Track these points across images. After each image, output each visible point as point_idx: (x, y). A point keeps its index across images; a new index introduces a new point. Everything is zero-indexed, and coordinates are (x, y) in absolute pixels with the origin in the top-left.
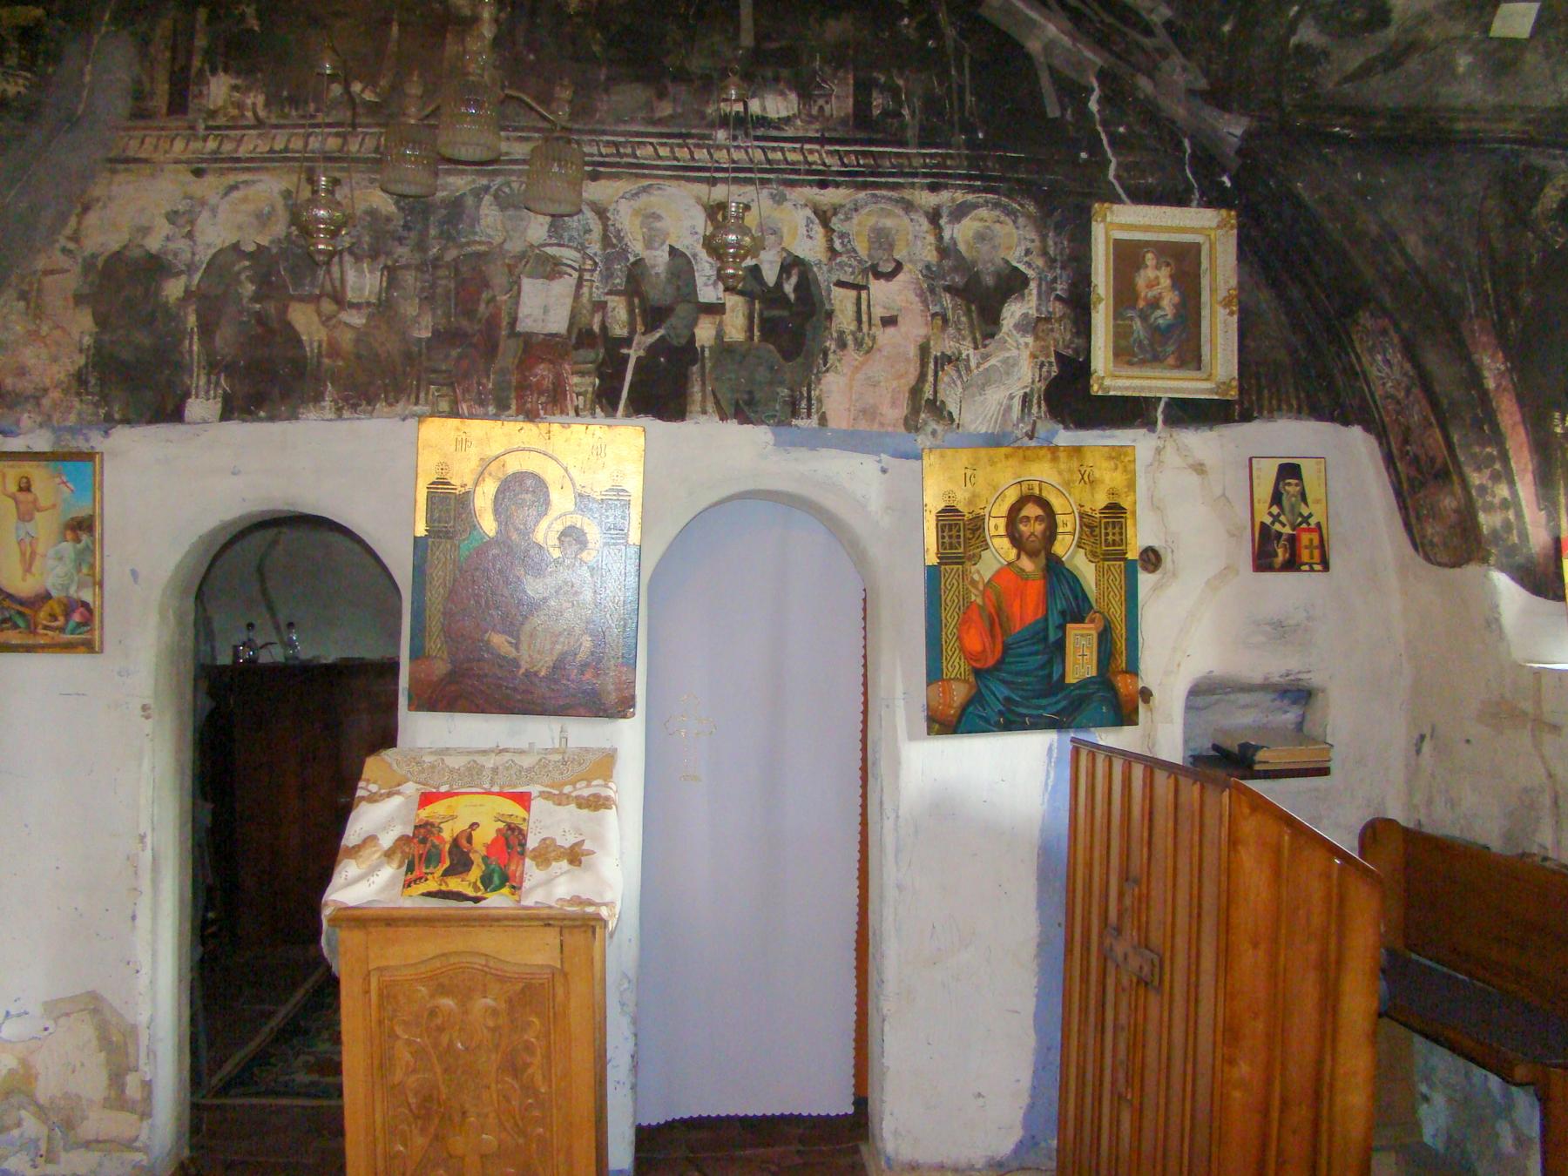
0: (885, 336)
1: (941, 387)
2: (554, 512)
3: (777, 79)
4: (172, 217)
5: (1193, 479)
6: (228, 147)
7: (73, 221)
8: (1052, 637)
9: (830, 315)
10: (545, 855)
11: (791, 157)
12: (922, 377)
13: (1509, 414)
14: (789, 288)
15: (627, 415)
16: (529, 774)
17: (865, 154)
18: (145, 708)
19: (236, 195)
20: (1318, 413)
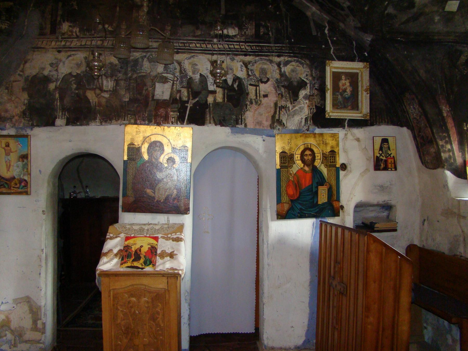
0: (264, 100)
1: (281, 115)
2: (165, 153)
3: (232, 24)
4: (51, 65)
5: (356, 143)
6: (68, 44)
7: (22, 66)
8: (314, 190)
9: (248, 94)
10: (163, 255)
11: (236, 47)
12: (275, 113)
13: (450, 124)
14: (235, 86)
15: (187, 124)
16: (158, 231)
17: (258, 46)
18: (43, 211)
19: (70, 58)
20: (394, 124)
